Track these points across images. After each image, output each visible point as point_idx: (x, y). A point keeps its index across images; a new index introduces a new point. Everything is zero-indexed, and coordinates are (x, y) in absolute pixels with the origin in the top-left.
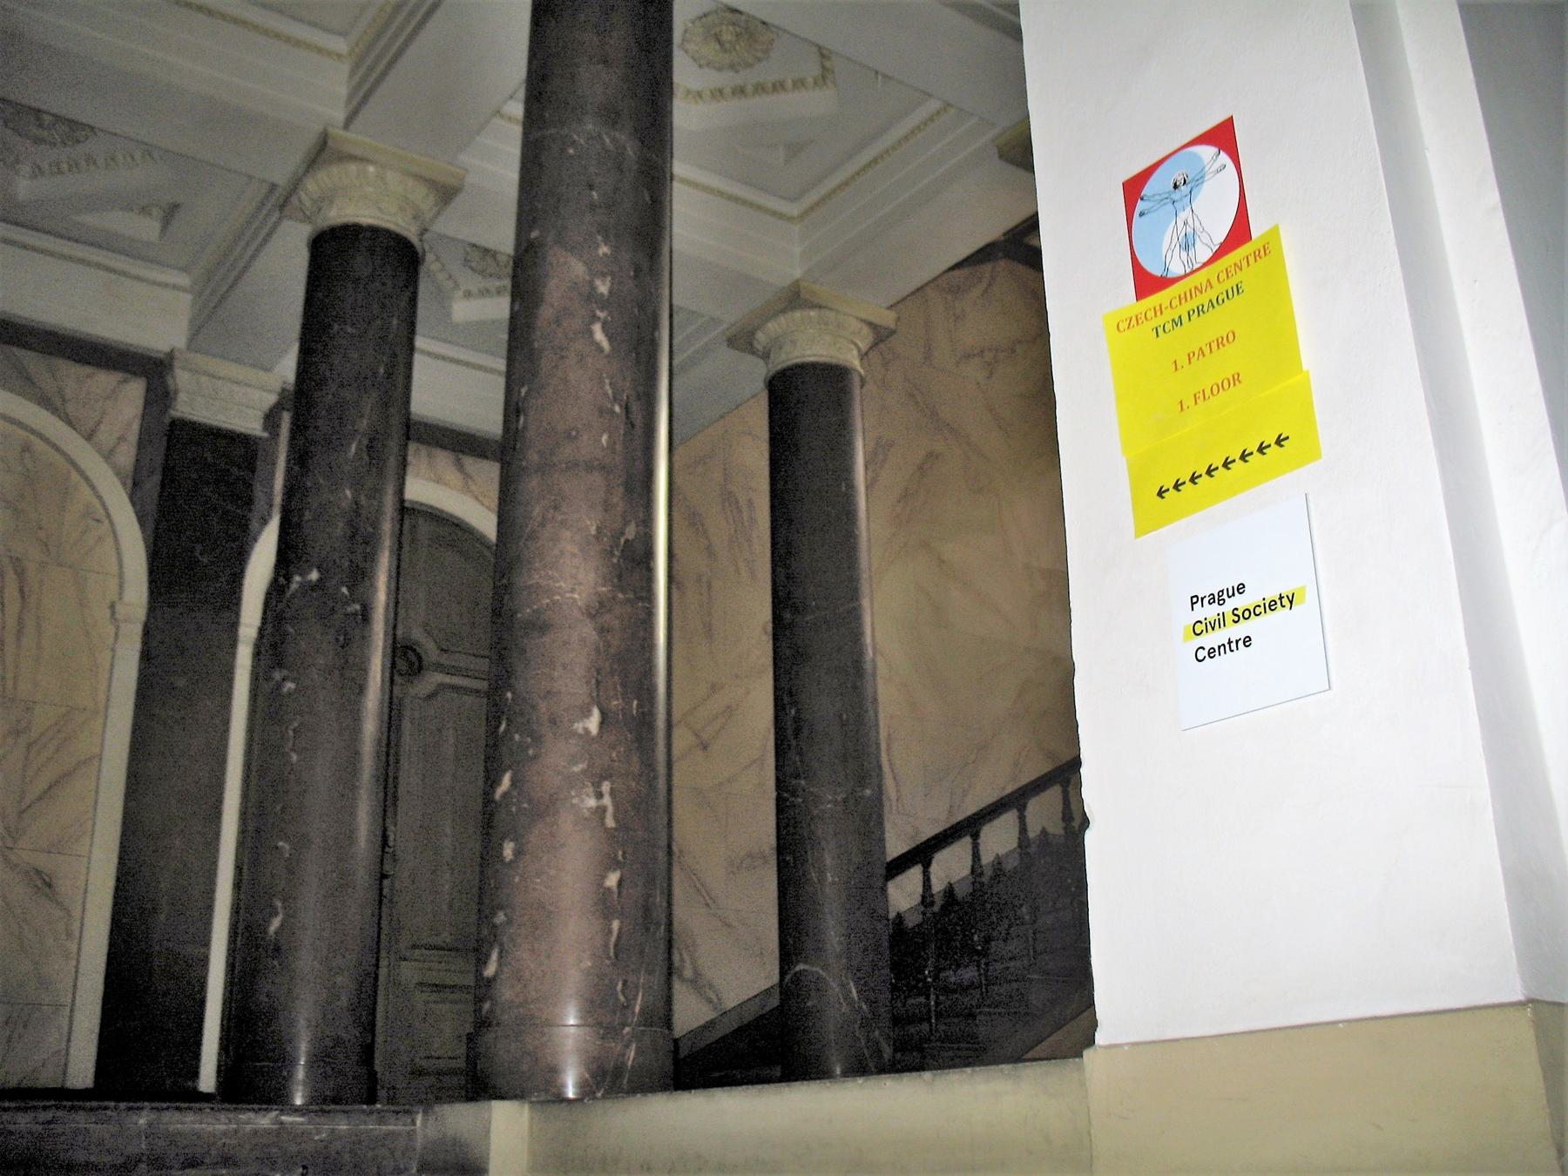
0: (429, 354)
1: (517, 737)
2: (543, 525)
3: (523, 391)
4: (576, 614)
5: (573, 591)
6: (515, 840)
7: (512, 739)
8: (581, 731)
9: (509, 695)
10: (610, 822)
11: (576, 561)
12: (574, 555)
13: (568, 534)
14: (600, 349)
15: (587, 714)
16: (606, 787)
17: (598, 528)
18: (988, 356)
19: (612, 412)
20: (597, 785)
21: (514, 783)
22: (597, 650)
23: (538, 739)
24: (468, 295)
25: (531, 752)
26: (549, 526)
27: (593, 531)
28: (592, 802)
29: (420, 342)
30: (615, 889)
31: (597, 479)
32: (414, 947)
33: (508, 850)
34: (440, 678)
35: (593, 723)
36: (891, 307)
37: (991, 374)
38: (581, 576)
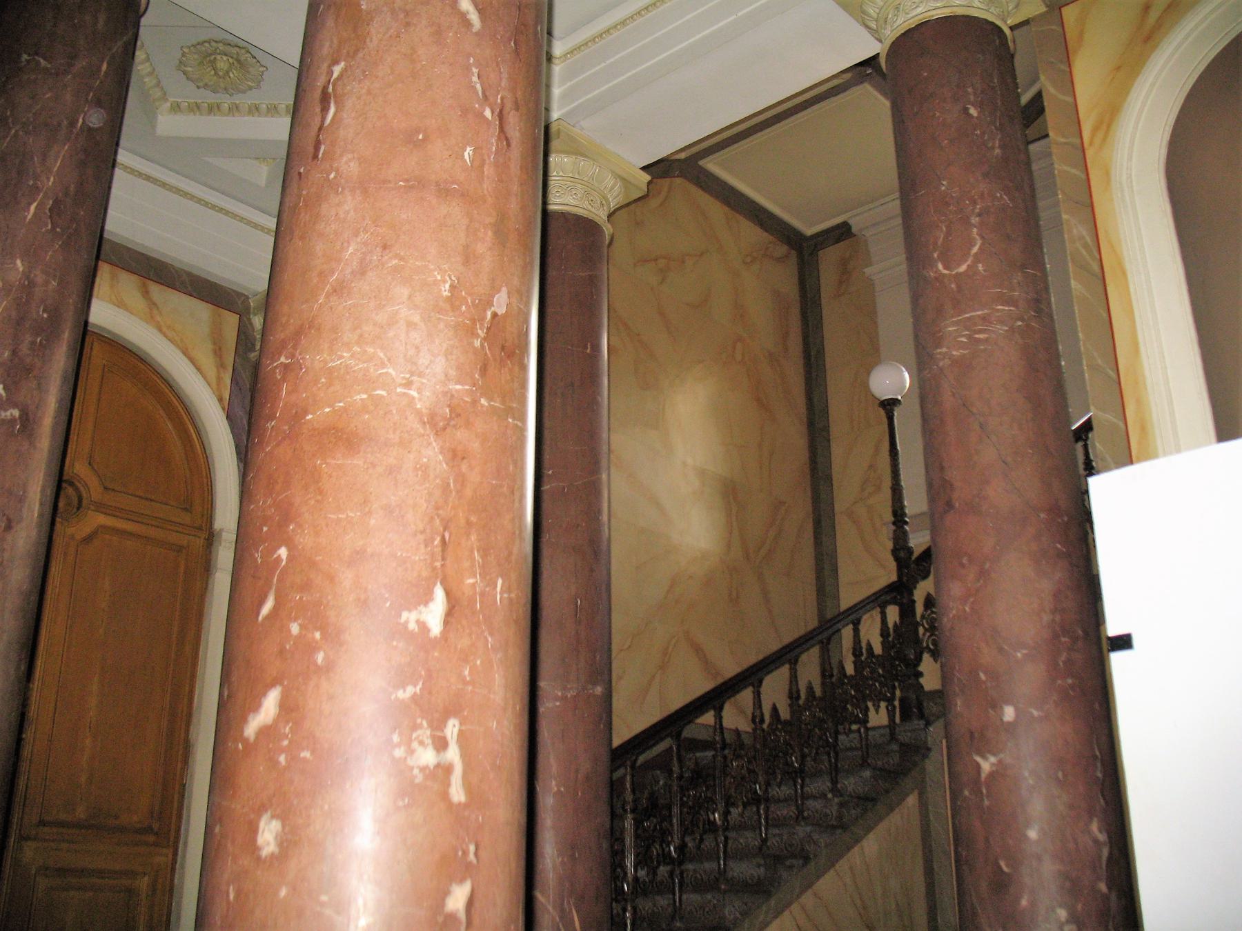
0: (132, 171)
1: (295, 628)
2: (362, 272)
3: (337, 70)
4: (413, 423)
5: (408, 384)
6: (283, 817)
7: (285, 629)
8: (412, 626)
9: (283, 552)
10: (457, 794)
11: (416, 336)
12: (410, 325)
13: (404, 292)
14: (467, 23)
15: (426, 598)
16: (452, 729)
17: (452, 287)
18: (662, 263)
19: (481, 115)
20: (438, 726)
21: (287, 708)
22: (445, 488)
23: (333, 636)
24: (176, 108)
25: (320, 658)
26: (370, 274)
27: (445, 290)
28: (428, 757)
29: (123, 157)
30: (462, 916)
31: (455, 211)
32: (42, 823)
33: (268, 834)
34: (102, 519)
35: (434, 614)
36: (644, 168)
37: (664, 279)
38: (424, 360)
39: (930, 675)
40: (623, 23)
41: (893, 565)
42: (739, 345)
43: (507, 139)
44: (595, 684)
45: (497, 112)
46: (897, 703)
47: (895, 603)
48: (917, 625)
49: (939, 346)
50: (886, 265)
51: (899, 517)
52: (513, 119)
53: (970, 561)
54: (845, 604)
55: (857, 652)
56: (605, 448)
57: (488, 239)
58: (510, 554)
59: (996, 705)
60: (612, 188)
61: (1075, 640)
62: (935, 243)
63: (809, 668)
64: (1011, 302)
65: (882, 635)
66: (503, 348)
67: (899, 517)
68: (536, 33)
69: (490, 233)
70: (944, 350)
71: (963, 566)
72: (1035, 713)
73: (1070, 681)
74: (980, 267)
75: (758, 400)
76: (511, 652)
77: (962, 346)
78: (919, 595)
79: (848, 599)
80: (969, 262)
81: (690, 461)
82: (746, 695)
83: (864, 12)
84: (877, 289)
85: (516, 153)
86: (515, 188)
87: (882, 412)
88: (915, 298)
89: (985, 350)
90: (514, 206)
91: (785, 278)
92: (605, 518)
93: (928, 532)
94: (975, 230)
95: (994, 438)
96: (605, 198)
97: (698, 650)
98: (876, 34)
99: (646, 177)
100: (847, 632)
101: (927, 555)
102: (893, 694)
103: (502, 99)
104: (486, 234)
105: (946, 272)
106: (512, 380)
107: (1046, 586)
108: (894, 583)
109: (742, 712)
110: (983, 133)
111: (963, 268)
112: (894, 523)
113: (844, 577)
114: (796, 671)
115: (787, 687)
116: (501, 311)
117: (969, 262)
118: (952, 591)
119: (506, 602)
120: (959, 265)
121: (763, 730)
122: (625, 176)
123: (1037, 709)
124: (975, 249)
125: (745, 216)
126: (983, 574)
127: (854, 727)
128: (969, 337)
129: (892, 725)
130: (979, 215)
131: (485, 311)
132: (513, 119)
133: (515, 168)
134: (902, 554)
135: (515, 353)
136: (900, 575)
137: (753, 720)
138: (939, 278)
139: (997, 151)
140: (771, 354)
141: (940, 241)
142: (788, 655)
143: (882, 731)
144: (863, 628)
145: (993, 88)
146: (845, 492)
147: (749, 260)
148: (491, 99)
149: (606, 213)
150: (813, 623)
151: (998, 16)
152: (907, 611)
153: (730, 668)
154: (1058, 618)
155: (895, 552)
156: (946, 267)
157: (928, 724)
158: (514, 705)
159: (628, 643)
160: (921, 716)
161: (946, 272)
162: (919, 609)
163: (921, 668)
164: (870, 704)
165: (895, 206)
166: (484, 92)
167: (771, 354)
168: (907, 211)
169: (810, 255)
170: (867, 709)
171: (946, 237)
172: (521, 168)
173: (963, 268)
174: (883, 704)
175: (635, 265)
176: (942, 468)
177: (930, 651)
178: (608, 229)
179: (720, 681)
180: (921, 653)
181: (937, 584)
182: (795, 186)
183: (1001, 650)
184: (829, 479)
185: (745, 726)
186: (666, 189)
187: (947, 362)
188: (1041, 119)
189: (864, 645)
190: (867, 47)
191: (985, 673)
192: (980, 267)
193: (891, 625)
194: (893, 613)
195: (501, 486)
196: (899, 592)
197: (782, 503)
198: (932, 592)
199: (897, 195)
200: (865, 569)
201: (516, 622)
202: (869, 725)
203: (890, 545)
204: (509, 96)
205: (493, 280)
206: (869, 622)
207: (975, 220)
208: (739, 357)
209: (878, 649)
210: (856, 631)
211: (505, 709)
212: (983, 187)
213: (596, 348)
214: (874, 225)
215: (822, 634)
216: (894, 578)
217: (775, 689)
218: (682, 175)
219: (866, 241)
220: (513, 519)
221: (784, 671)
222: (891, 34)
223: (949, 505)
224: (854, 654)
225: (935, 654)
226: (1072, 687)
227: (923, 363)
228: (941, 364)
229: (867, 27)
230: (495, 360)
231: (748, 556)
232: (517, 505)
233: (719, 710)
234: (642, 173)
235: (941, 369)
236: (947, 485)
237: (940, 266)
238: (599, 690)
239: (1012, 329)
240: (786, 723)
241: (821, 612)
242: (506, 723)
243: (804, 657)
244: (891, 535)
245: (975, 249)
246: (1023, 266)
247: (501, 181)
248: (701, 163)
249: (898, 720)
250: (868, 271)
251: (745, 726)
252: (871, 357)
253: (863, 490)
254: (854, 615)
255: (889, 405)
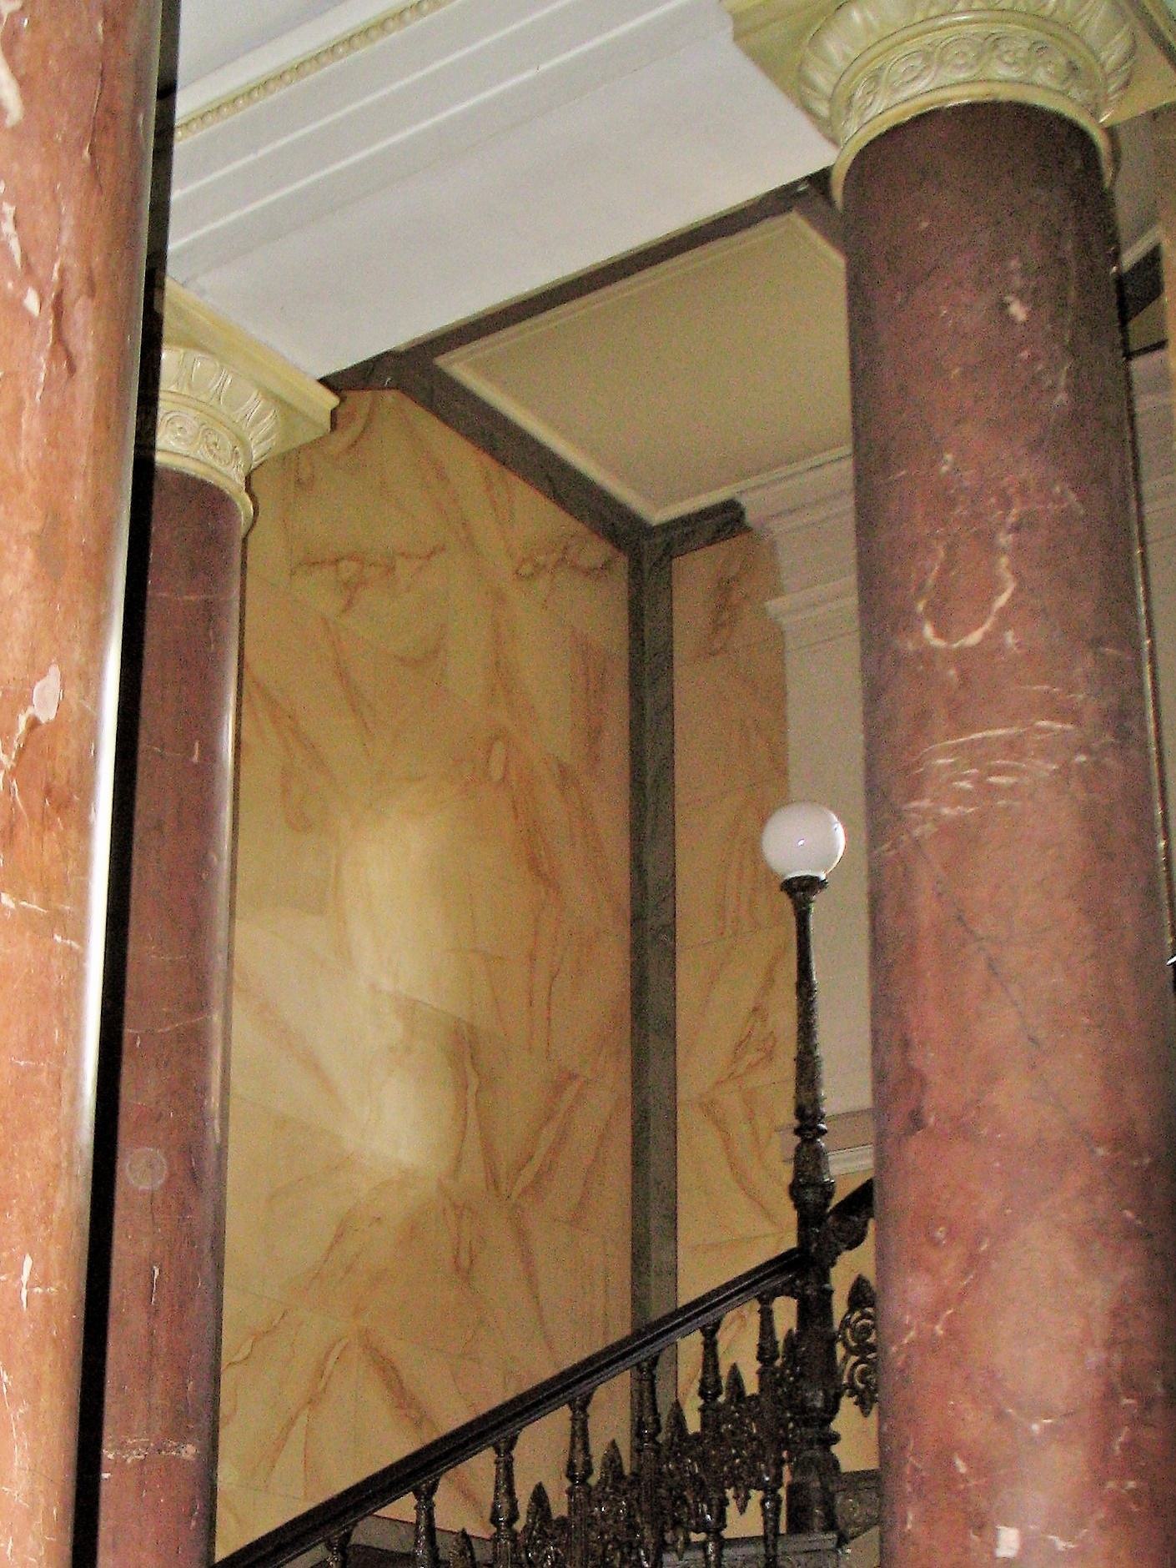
18: (348, 569)
19: (17, 306)
37: (349, 603)
39: (854, 1440)
40: (299, 69)
41: (791, 1216)
42: (499, 749)
43: (69, 357)
44: (183, 1440)
45: (49, 301)
46: (782, 1492)
47: (791, 1294)
48: (832, 1341)
49: (914, 793)
50: (812, 597)
51: (808, 1122)
52: (81, 314)
53: (951, 1235)
54: (688, 1293)
55: (708, 1390)
56: (221, 958)
57: (26, 566)
58: (50, 1207)
59: (982, 1525)
60: (257, 421)
61: (1147, 1404)
62: (920, 588)
63: (611, 1414)
64: (1069, 713)
65: (760, 1358)
66: (48, 792)
67: (808, 1122)
68: (134, 129)
69: (29, 555)
70: (926, 803)
71: (935, 1244)
72: (1061, 1545)
73: (1131, 1484)
74: (1010, 638)
75: (534, 863)
76: (44, 1402)
77: (962, 797)
78: (841, 1279)
79: (695, 1280)
80: (987, 626)
81: (386, 983)
82: (481, 1466)
83: (805, 80)
84: (791, 646)
85: (86, 384)
86: (83, 460)
87: (786, 904)
88: (874, 693)
89: (1008, 808)
90: (78, 496)
91: (598, 610)
92: (214, 1102)
93: (869, 1150)
94: (1004, 561)
95: (1014, 989)
96: (240, 440)
97: (387, 1370)
98: (829, 130)
99: (331, 400)
100: (690, 1346)
101: (863, 1199)
102: (778, 1479)
103: (62, 272)
104: (21, 553)
105: (938, 643)
106: (65, 856)
107: (1099, 1294)
108: (791, 1252)
109: (468, 1496)
110: (1034, 358)
111: (974, 638)
112: (798, 1132)
113: (689, 1230)
114: (584, 1423)
115: (565, 1458)
116: (47, 715)
117: (987, 626)
118: (907, 1284)
119: (38, 1304)
120: (967, 632)
121: (514, 1536)
122: (284, 394)
123: (1063, 1538)
124: (1002, 600)
125: (525, 478)
126: (974, 1261)
127: (695, 1537)
128: (979, 781)
129: (770, 1537)
130: (1016, 528)
131: (15, 716)
132: (81, 314)
133: (83, 417)
134: (810, 1196)
135: (68, 803)
136: (803, 1237)
137: (494, 1520)
138: (926, 655)
139: (1062, 397)
140: (563, 770)
141: (930, 582)
142: (570, 1388)
143: (751, 1550)
144: (723, 1338)
145: (1062, 262)
146: (700, 1065)
147: (527, 569)
148: (40, 272)
149: (242, 473)
150: (620, 1330)
151: (1084, 106)
152: (814, 1310)
153: (452, 1415)
154: (1117, 1359)
155: (795, 1191)
156: (939, 634)
157: (842, 1540)
158: (48, 1510)
159: (246, 1351)
160: (830, 1525)
161: (938, 643)
162: (839, 1307)
163: (835, 1426)
164: (730, 1493)
165: (840, 470)
166: (25, 257)
167: (563, 770)
168: (867, 518)
169: (654, 564)
170: (724, 1502)
171: (944, 571)
172: (96, 419)
173: (974, 638)
174: (756, 1495)
175: (293, 573)
176: (906, 1044)
177: (854, 1391)
178: (244, 505)
179: (429, 1437)
180: (838, 1397)
181: (881, 1255)
182: (632, 429)
183: (1000, 1415)
184: (669, 1028)
185: (479, 1528)
186: (364, 411)
187: (929, 828)
188: (1151, 308)
189: (724, 1371)
190: (804, 153)
191: (966, 1459)
192: (1010, 638)
193: (780, 1336)
194: (785, 1314)
195: (38, 1071)
196: (800, 1270)
197: (572, 1077)
198: (870, 1275)
199: (847, 449)
200: (733, 1223)
201: (55, 1342)
202: (727, 1534)
203: (787, 1176)
204: (74, 264)
205: (33, 650)
206: (734, 1327)
207: (1005, 539)
208: (497, 774)
209: (751, 1387)
210: (710, 1346)
211: (30, 1515)
212: (1027, 472)
213: (211, 753)
214: (791, 511)
215: (641, 1348)
216: (791, 1242)
217: (541, 1452)
218: (398, 386)
219: (773, 544)
220: (57, 1138)
221: (559, 1419)
222: (859, 132)
223: (916, 1120)
224: (702, 1394)
225: (864, 1404)
226: (1135, 1495)
227: (881, 810)
228: (917, 832)
229: (809, 111)
230: (31, 815)
231: (493, 1189)
232: (65, 1109)
233: (425, 1498)
234: (321, 388)
235: (917, 843)
236: (914, 1078)
237: (928, 631)
238: (189, 1451)
239: (1066, 770)
240: (563, 1523)
241: (638, 1301)
242: (31, 1542)
243: (601, 1394)
244: (791, 1154)
245: (1002, 600)
246: (1098, 642)
247: (54, 444)
248: (441, 361)
249: (783, 1529)
250: (773, 605)
251: (479, 1528)
252: (769, 788)
253: (736, 1057)
254: (704, 1313)
255: (802, 890)
